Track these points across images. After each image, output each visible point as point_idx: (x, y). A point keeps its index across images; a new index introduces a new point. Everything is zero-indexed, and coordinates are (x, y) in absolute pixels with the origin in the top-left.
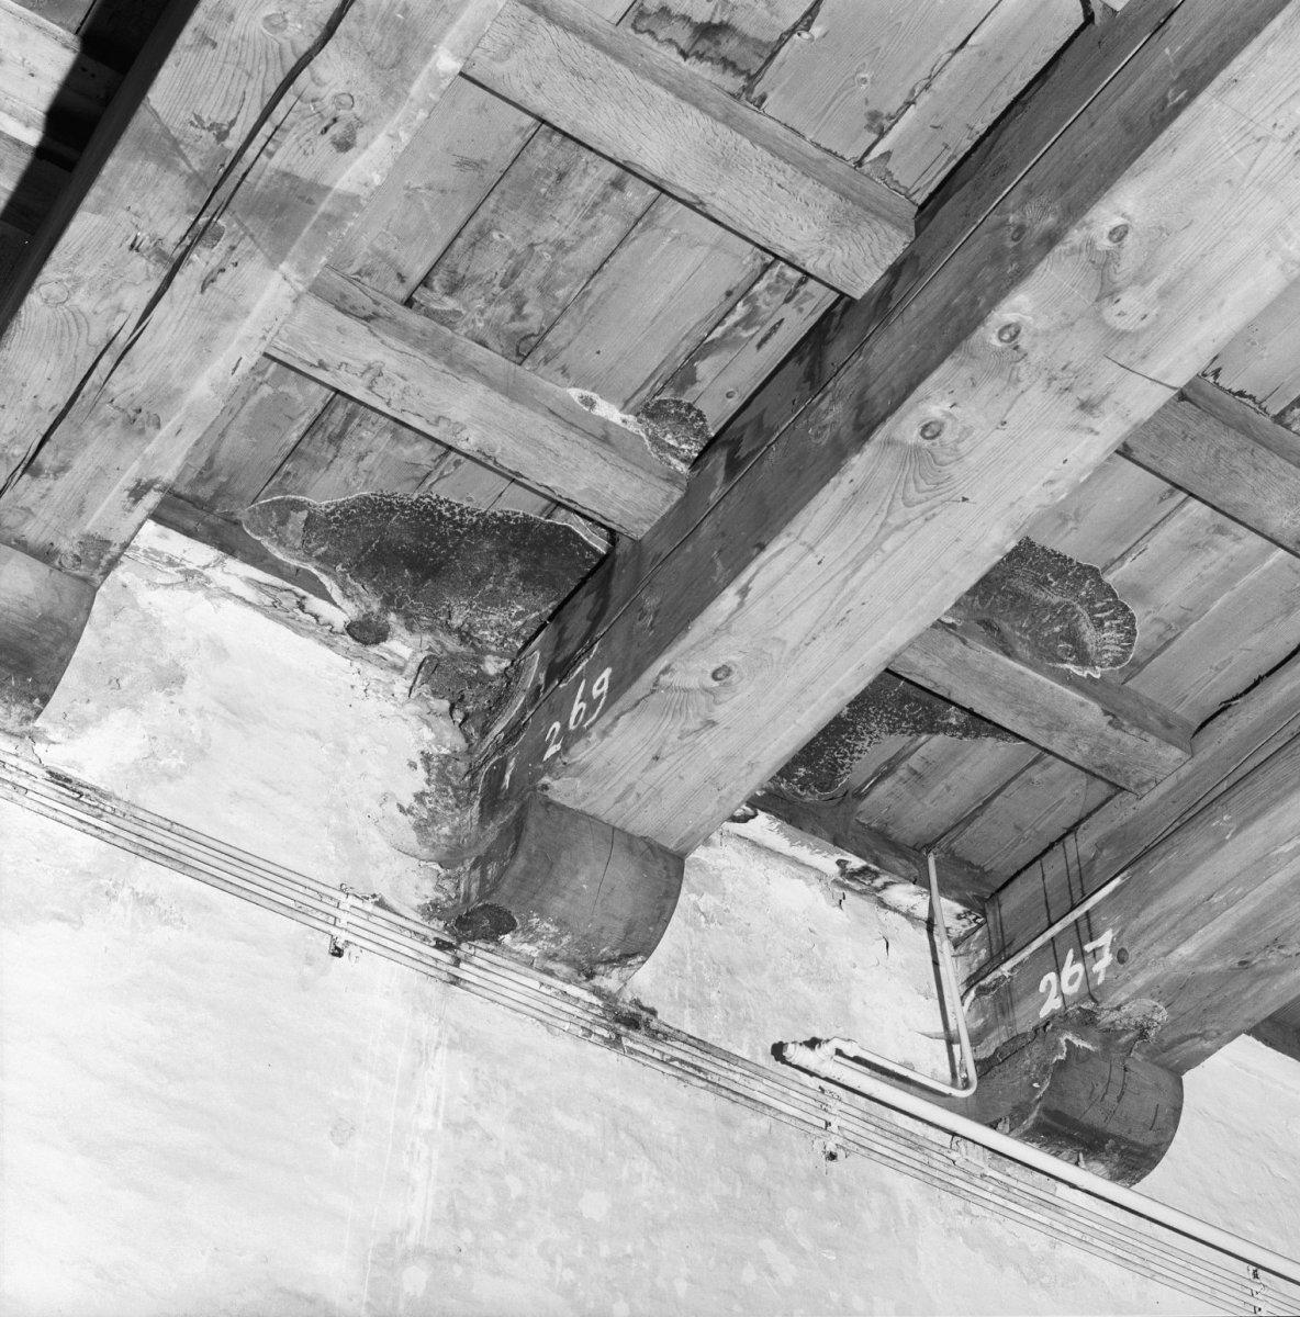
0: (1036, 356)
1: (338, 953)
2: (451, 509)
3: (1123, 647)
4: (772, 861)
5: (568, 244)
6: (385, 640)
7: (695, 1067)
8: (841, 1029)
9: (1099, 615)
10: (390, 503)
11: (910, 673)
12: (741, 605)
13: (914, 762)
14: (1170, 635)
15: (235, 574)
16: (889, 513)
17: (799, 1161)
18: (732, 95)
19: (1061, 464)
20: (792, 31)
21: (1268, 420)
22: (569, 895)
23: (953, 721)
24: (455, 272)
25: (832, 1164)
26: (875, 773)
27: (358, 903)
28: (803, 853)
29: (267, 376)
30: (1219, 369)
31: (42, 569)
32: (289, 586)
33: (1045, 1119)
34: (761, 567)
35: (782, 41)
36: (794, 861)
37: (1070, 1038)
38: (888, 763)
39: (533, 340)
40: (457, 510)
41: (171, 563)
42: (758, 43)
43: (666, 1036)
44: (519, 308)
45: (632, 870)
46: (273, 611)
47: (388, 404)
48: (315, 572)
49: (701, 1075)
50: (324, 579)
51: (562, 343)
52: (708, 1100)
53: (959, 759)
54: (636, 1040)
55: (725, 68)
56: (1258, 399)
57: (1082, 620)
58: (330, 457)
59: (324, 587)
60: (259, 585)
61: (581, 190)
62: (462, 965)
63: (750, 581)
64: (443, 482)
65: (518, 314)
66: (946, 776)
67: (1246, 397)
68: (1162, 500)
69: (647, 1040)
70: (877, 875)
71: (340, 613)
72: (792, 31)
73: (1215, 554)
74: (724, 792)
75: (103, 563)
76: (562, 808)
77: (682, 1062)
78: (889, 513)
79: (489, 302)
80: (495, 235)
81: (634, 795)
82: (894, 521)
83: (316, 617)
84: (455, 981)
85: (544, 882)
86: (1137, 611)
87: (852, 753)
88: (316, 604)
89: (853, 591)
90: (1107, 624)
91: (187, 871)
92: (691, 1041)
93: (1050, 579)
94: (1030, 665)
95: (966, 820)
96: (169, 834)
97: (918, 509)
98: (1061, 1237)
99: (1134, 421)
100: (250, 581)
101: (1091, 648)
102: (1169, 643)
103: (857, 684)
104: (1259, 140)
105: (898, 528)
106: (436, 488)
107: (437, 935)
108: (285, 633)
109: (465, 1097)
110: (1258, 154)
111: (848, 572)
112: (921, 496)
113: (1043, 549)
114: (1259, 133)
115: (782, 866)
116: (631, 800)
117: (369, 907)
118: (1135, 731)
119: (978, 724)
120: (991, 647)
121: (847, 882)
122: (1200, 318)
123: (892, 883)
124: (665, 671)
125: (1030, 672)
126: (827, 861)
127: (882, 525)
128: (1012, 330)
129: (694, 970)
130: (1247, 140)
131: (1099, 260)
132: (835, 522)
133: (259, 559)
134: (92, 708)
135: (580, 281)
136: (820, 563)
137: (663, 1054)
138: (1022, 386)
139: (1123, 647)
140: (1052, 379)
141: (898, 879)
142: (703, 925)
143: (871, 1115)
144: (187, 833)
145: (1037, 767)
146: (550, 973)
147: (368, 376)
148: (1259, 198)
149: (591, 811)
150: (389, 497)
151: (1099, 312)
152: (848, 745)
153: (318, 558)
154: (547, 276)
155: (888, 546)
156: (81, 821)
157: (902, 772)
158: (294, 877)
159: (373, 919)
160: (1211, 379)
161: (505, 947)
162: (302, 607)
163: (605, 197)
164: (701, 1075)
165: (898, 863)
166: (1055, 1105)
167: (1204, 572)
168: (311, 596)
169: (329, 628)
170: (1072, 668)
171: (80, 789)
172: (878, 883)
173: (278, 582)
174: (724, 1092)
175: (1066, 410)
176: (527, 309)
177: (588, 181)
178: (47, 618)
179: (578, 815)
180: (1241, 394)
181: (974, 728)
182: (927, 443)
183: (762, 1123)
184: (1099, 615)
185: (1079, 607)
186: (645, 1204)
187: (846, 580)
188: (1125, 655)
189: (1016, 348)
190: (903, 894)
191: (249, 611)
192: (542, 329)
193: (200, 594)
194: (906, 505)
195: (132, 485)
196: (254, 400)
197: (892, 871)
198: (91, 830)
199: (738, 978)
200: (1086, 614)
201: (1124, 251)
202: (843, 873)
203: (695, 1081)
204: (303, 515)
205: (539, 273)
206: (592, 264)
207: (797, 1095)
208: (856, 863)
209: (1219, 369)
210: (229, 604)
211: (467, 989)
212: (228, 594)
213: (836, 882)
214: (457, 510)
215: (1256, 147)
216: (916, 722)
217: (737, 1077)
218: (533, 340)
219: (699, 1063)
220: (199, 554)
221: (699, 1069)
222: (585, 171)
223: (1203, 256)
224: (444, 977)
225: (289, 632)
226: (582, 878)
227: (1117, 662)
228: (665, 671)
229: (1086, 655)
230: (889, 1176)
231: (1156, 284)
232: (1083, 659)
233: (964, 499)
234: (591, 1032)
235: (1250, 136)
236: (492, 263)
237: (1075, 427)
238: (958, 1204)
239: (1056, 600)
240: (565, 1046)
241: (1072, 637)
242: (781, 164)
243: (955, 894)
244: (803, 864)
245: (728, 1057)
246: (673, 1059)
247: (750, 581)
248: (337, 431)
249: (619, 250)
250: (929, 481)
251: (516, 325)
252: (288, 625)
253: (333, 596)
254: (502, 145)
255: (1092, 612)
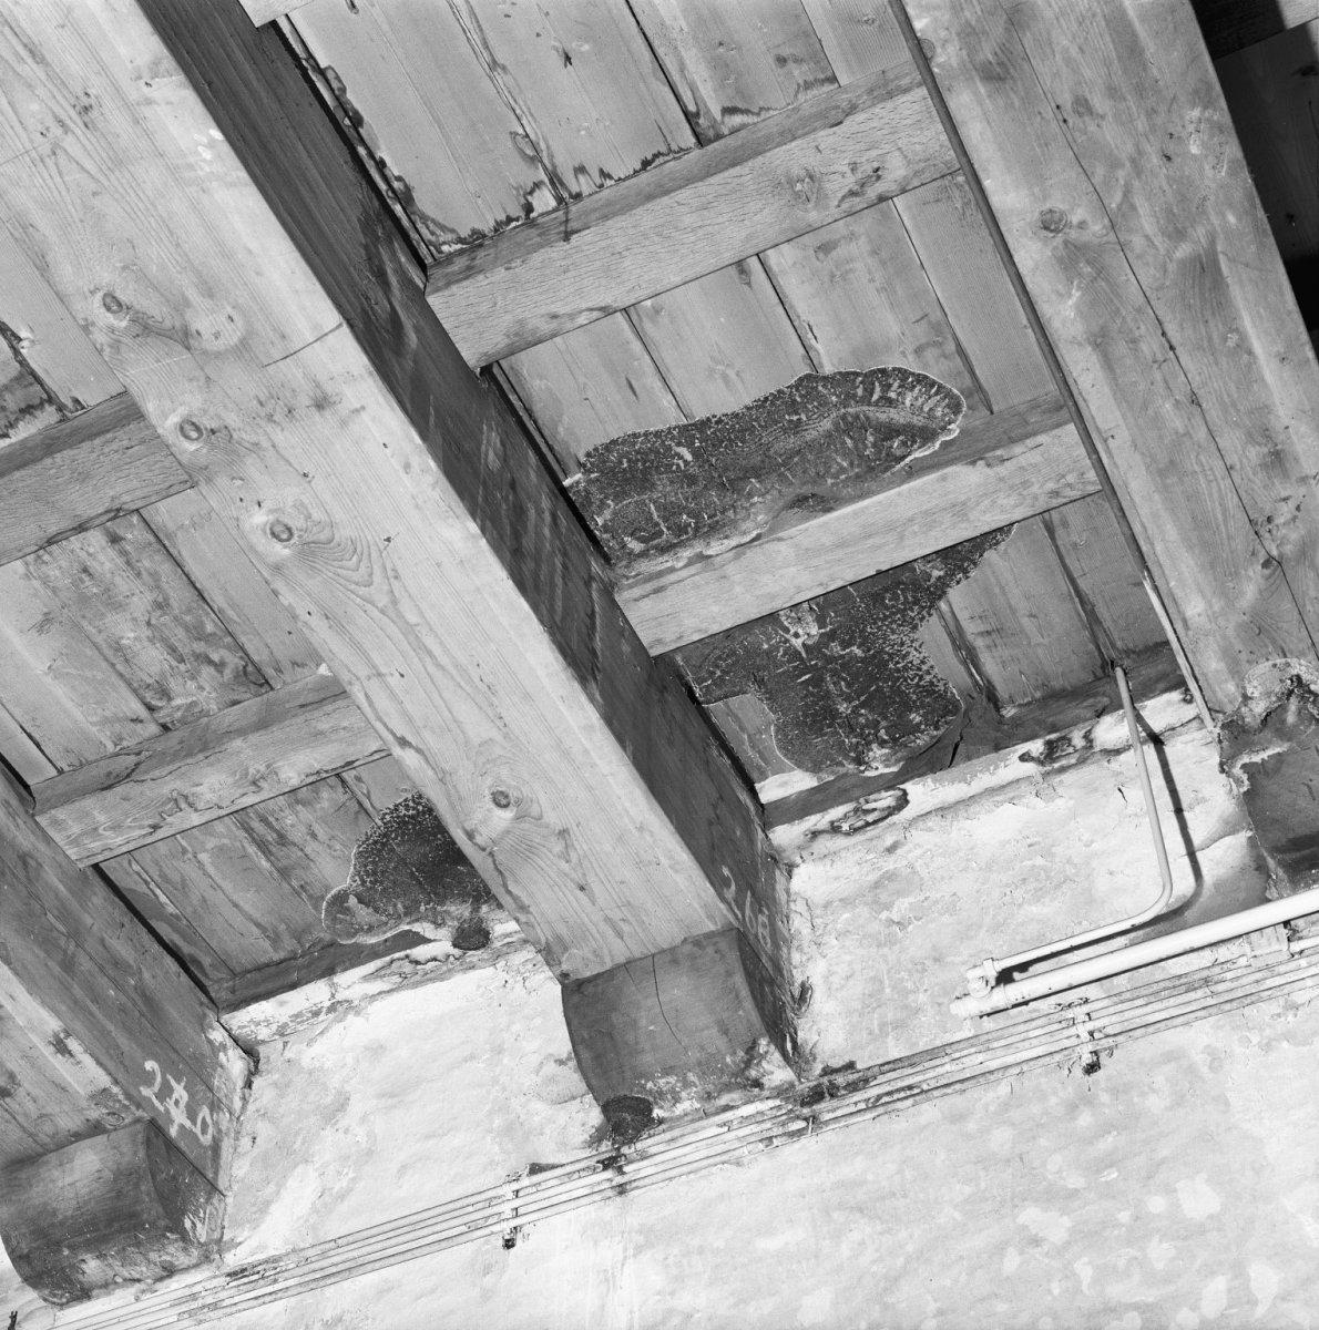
0: (232, 419)
1: (509, 1244)
2: (407, 807)
3: (936, 394)
4: (974, 808)
5: (160, 599)
6: (489, 933)
7: (903, 1089)
8: (1085, 923)
9: (875, 397)
10: (375, 842)
11: (791, 598)
12: (418, 751)
13: (970, 628)
14: (951, 347)
15: (351, 982)
16: (373, 603)
17: (1053, 1100)
18: (61, 421)
19: (387, 450)
20: (16, 352)
21: (696, 153)
22: (647, 1047)
23: (936, 573)
24: (149, 686)
25: (1095, 1076)
26: (964, 663)
27: (515, 1186)
28: (984, 780)
29: (189, 849)
30: (601, 171)
31: (102, 1139)
32: (388, 959)
33: (1288, 857)
34: (380, 719)
35: (23, 362)
36: (991, 791)
37: (1246, 759)
38: (957, 647)
39: (250, 668)
40: (411, 804)
41: (316, 1014)
42: (18, 379)
43: (866, 1081)
44: (210, 662)
45: (685, 979)
46: (406, 982)
47: (220, 808)
48: (407, 928)
49: (916, 1091)
50: (417, 927)
51: (266, 652)
52: (929, 1111)
53: (997, 590)
54: (825, 1108)
55: (31, 414)
56: (663, 149)
57: (871, 415)
58: (300, 853)
59: (417, 934)
60: (375, 975)
61: (108, 565)
62: (625, 1169)
63: (394, 735)
64: (373, 797)
65: (219, 666)
66: (1013, 611)
67: (653, 160)
68: (749, 284)
69: (835, 1103)
70: (1067, 740)
71: (440, 943)
72: (16, 352)
73: (858, 265)
74: (663, 860)
75: (127, 1103)
76: (589, 980)
77: (889, 1093)
78: (373, 603)
79: (193, 678)
80: (124, 642)
81: (621, 924)
82: (383, 601)
83: (435, 959)
84: (622, 1190)
85: (618, 1054)
86: (892, 362)
87: (920, 669)
88: (420, 952)
89: (457, 666)
90: (893, 395)
91: (354, 1272)
92: (886, 1068)
93: (795, 418)
94: (862, 497)
95: (1092, 619)
96: (340, 1250)
97: (378, 577)
98: (1287, 988)
99: (364, 372)
100: (366, 978)
101: (918, 421)
102: (961, 351)
103: (582, 708)
104: (54, 154)
105: (395, 602)
106: (378, 806)
107: (596, 1159)
108: (431, 988)
109: (659, 1293)
110: (71, 158)
111: (428, 660)
112: (363, 569)
113: (748, 408)
114: (46, 149)
115: (987, 803)
116: (626, 928)
117: (526, 1181)
118: (1018, 449)
119: (960, 557)
120: (808, 519)
121: (1056, 765)
122: (257, 274)
123: (1090, 731)
124: (470, 835)
125: (867, 502)
126: (1011, 766)
127: (382, 612)
128: (187, 427)
129: (894, 988)
130: (50, 162)
131: (137, 329)
132: (357, 646)
133: (358, 956)
134: (272, 1188)
135: (204, 610)
136: (402, 676)
137: (867, 1100)
138: (265, 444)
139: (936, 394)
140: (270, 418)
141: (1093, 722)
142: (900, 935)
143: (1120, 994)
144: (350, 1239)
145: (1060, 532)
146: (727, 1108)
147: (183, 806)
148: (128, 176)
149: (622, 960)
150: (367, 839)
151: (205, 352)
152: (905, 668)
153: (406, 914)
154: (187, 629)
155: (412, 618)
156: (256, 1298)
157: (979, 643)
158: (451, 1206)
159: (544, 1186)
160: (609, 182)
161: (661, 1121)
162: (417, 963)
163: (123, 553)
164: (916, 1091)
165: (1081, 711)
166: (1280, 837)
167: (877, 284)
168: (408, 951)
169: (452, 959)
170: (917, 455)
171: (256, 1270)
172: (1078, 740)
173: (378, 963)
174: (936, 1093)
175: (323, 424)
176: (215, 657)
177: (101, 557)
178: (119, 1174)
179: (609, 975)
180: (646, 164)
181: (963, 560)
182: (295, 539)
183: (1003, 1089)
184: (875, 397)
185: (850, 410)
186: (874, 1268)
187: (439, 666)
188: (949, 394)
189: (213, 432)
190: (1112, 730)
191: (396, 996)
192: (241, 658)
193: (350, 1017)
194: (369, 585)
195: (52, 1048)
196: (211, 870)
197: (1074, 723)
198: (267, 1299)
199: (949, 959)
200: (865, 408)
201: (135, 303)
202: (1041, 763)
203: (899, 1105)
204: (353, 901)
205: (181, 633)
206: (189, 594)
207: (1037, 1033)
208: (1036, 747)
209: (601, 171)
210: (378, 1005)
211: (637, 1188)
212: (373, 998)
213: (1046, 775)
214: (411, 804)
215: (62, 159)
216: (915, 603)
217: (948, 1067)
218: (250, 668)
219: (900, 1084)
220: (315, 993)
221: (910, 1087)
222: (90, 555)
223: (178, 245)
224: (610, 1193)
225: (437, 984)
226: (643, 1022)
227: (955, 408)
228: (470, 835)
229: (923, 429)
230: (1172, 1038)
231: (192, 294)
232: (927, 435)
233: (388, 540)
234: (770, 1139)
235: (47, 160)
236: (152, 660)
237: (344, 423)
238: (1274, 1007)
239: (827, 424)
240: (761, 1165)
241: (889, 431)
242: (109, 436)
243: (1161, 686)
244: (1004, 787)
245: (933, 1053)
246: (879, 1097)
247: (394, 735)
248: (275, 835)
249: (186, 569)
250: (347, 557)
251: (228, 673)
252: (432, 980)
253: (427, 935)
254: (35, 595)
255: (866, 400)
